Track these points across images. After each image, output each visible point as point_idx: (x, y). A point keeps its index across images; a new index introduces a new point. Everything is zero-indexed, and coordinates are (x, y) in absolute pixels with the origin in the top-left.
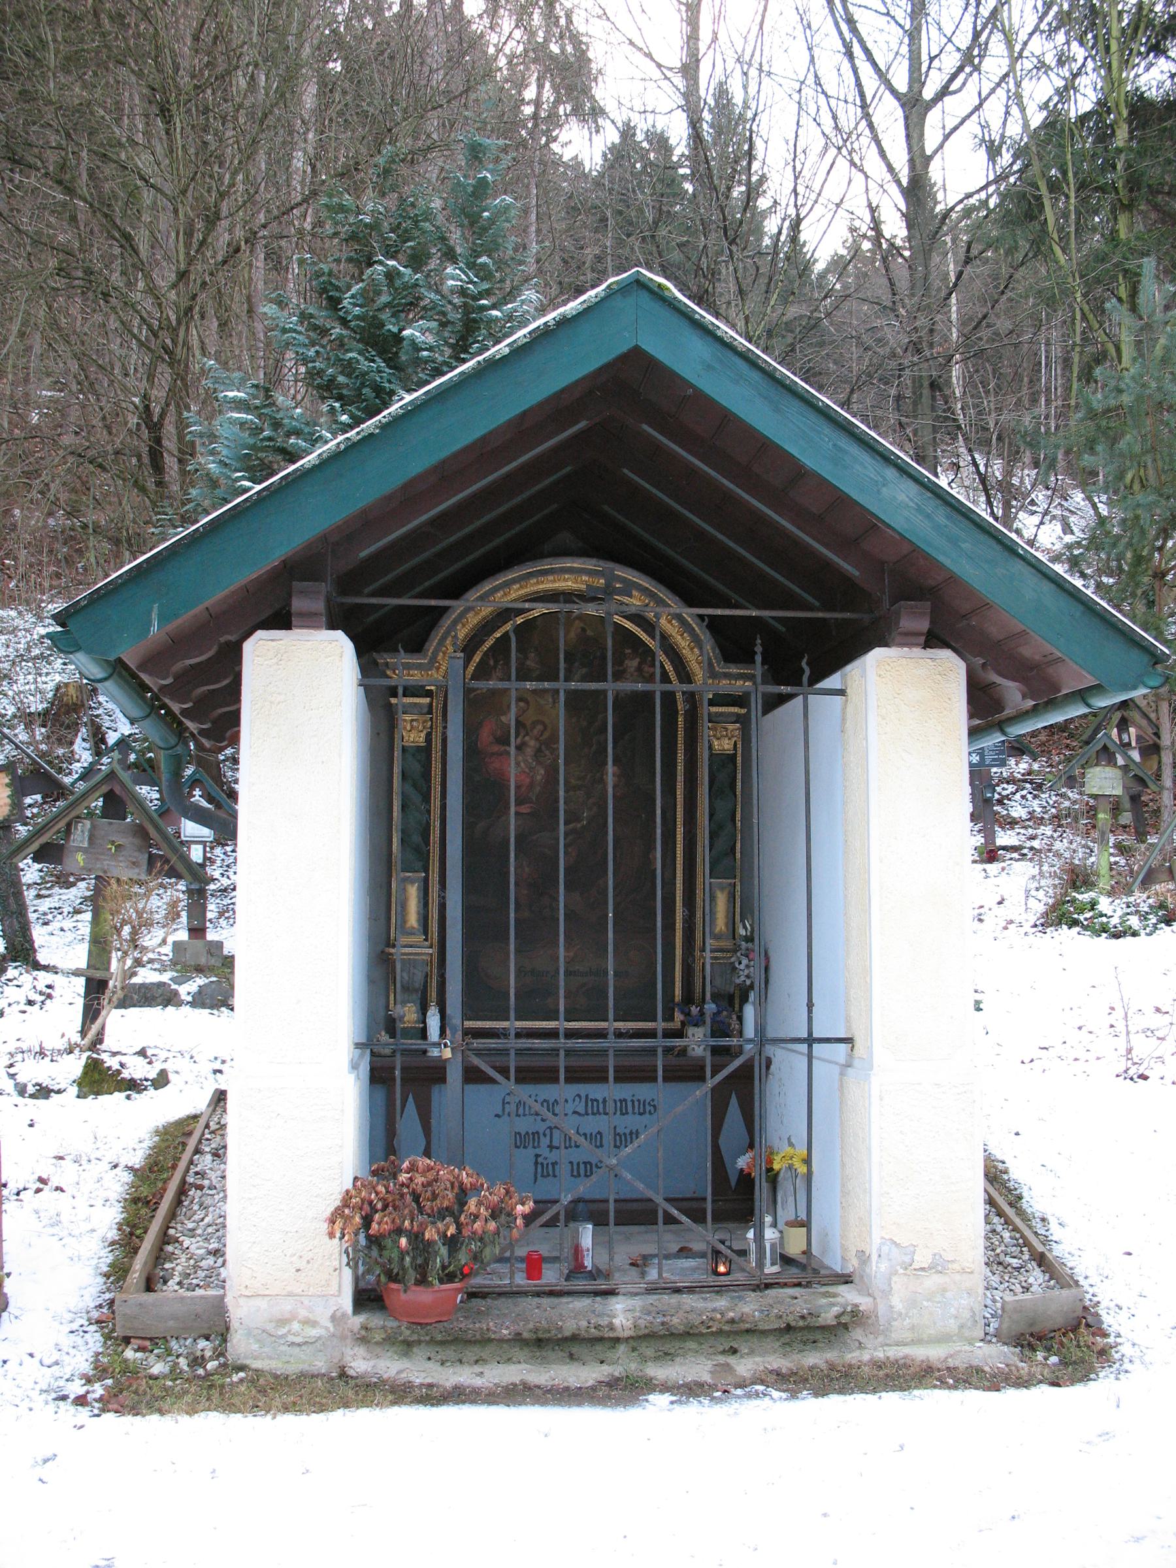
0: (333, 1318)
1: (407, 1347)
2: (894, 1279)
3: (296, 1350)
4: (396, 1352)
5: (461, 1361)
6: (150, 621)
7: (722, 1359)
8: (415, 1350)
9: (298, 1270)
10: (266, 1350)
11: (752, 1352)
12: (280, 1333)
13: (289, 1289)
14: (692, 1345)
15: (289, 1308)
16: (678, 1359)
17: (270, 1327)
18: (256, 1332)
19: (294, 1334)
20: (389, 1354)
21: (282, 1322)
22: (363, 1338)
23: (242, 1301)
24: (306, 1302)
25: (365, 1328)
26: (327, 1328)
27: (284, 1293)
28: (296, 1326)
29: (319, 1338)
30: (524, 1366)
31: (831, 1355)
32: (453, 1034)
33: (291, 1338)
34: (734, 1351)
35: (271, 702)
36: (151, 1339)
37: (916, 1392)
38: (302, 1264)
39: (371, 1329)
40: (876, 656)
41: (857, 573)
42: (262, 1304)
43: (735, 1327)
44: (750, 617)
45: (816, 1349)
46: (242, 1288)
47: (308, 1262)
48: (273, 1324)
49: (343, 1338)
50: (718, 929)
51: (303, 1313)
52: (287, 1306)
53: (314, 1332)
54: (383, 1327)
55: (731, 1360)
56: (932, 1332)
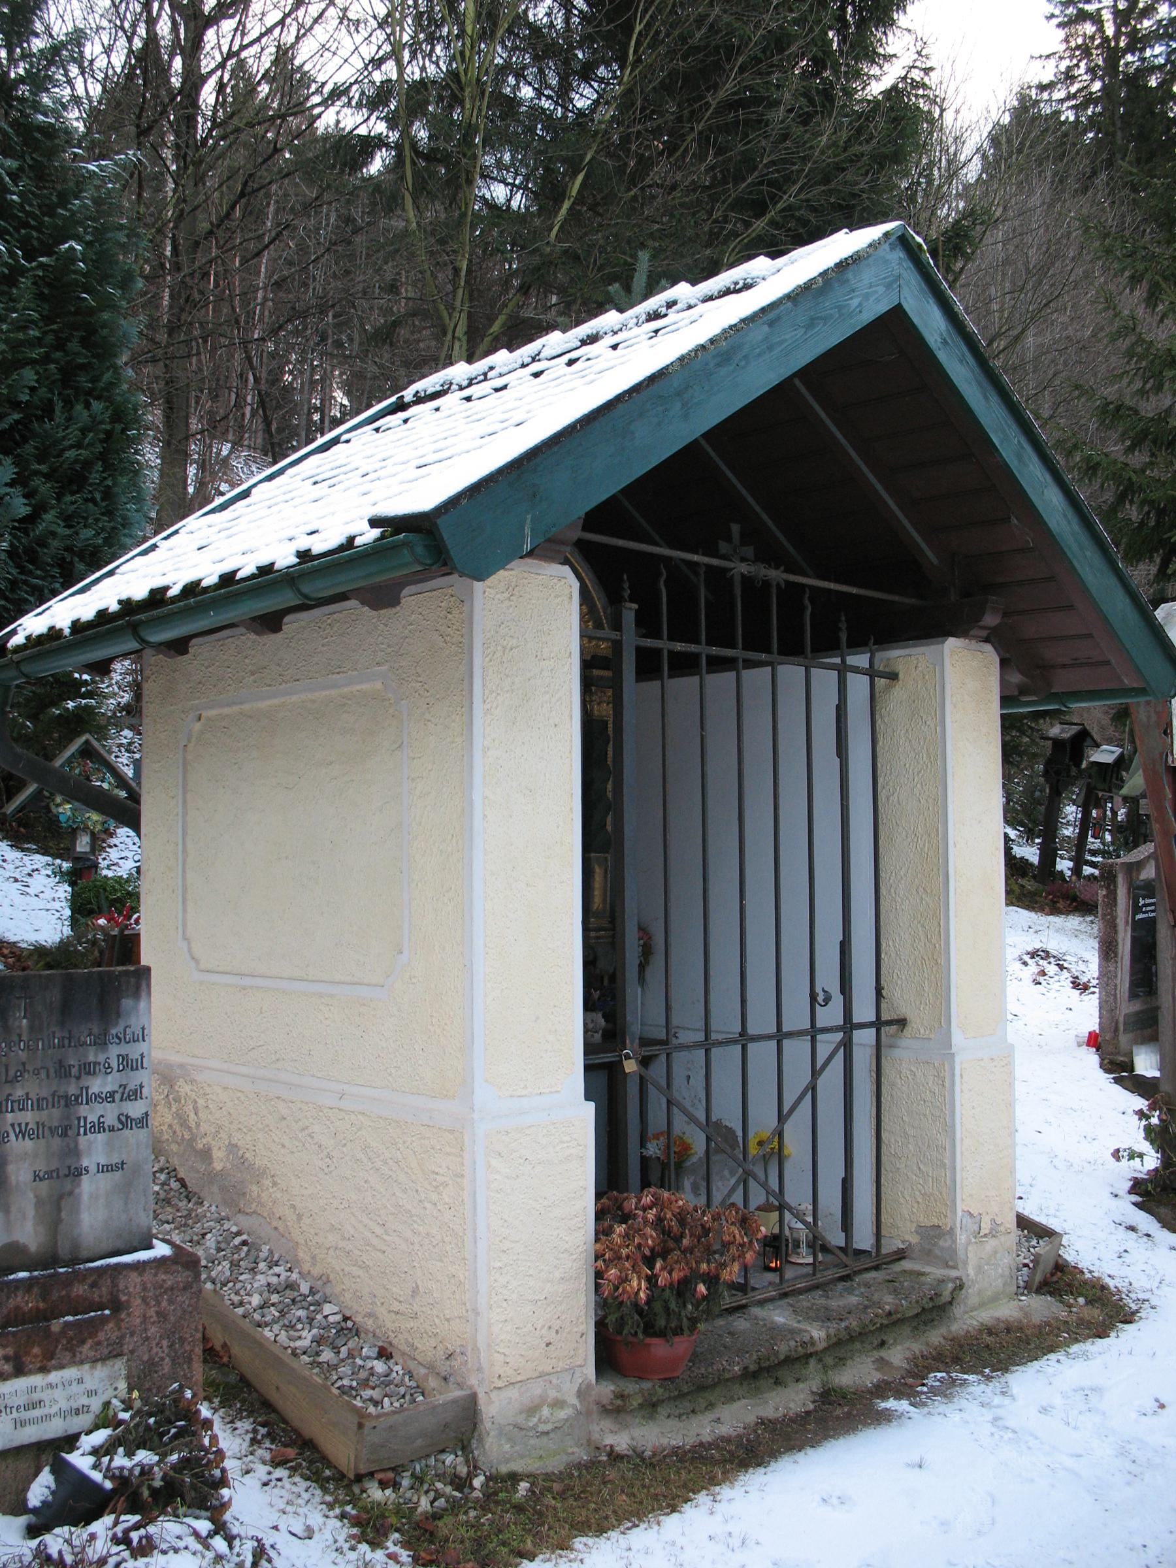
0: (580, 1393)
1: (651, 1407)
2: (970, 1248)
3: (545, 1439)
4: (643, 1417)
5: (693, 1411)
6: (523, 536)
7: (876, 1354)
8: (659, 1409)
9: (548, 1345)
10: (517, 1448)
11: (895, 1343)
12: (531, 1424)
13: (540, 1368)
14: (858, 1345)
15: (538, 1391)
16: (849, 1362)
17: (520, 1420)
18: (507, 1428)
19: (544, 1422)
20: (637, 1420)
21: (532, 1410)
22: (616, 1410)
23: (494, 1395)
24: (555, 1381)
25: (621, 1396)
26: (574, 1406)
27: (537, 1374)
28: (546, 1411)
29: (567, 1420)
30: (744, 1402)
31: (943, 1330)
32: (632, 1042)
33: (543, 1428)
34: (883, 1344)
35: (504, 648)
36: (393, 1469)
37: (1075, 1348)
38: (551, 1336)
39: (629, 1396)
40: (951, 642)
41: (935, 561)
42: (513, 1393)
43: (894, 1317)
44: (851, 594)
45: (1006, 1321)
46: (495, 1380)
47: (557, 1332)
48: (524, 1415)
49: (589, 1413)
50: (595, 907)
51: (552, 1394)
52: (536, 1390)
53: (563, 1414)
54: (641, 1390)
55: (883, 1353)
56: (989, 1293)
